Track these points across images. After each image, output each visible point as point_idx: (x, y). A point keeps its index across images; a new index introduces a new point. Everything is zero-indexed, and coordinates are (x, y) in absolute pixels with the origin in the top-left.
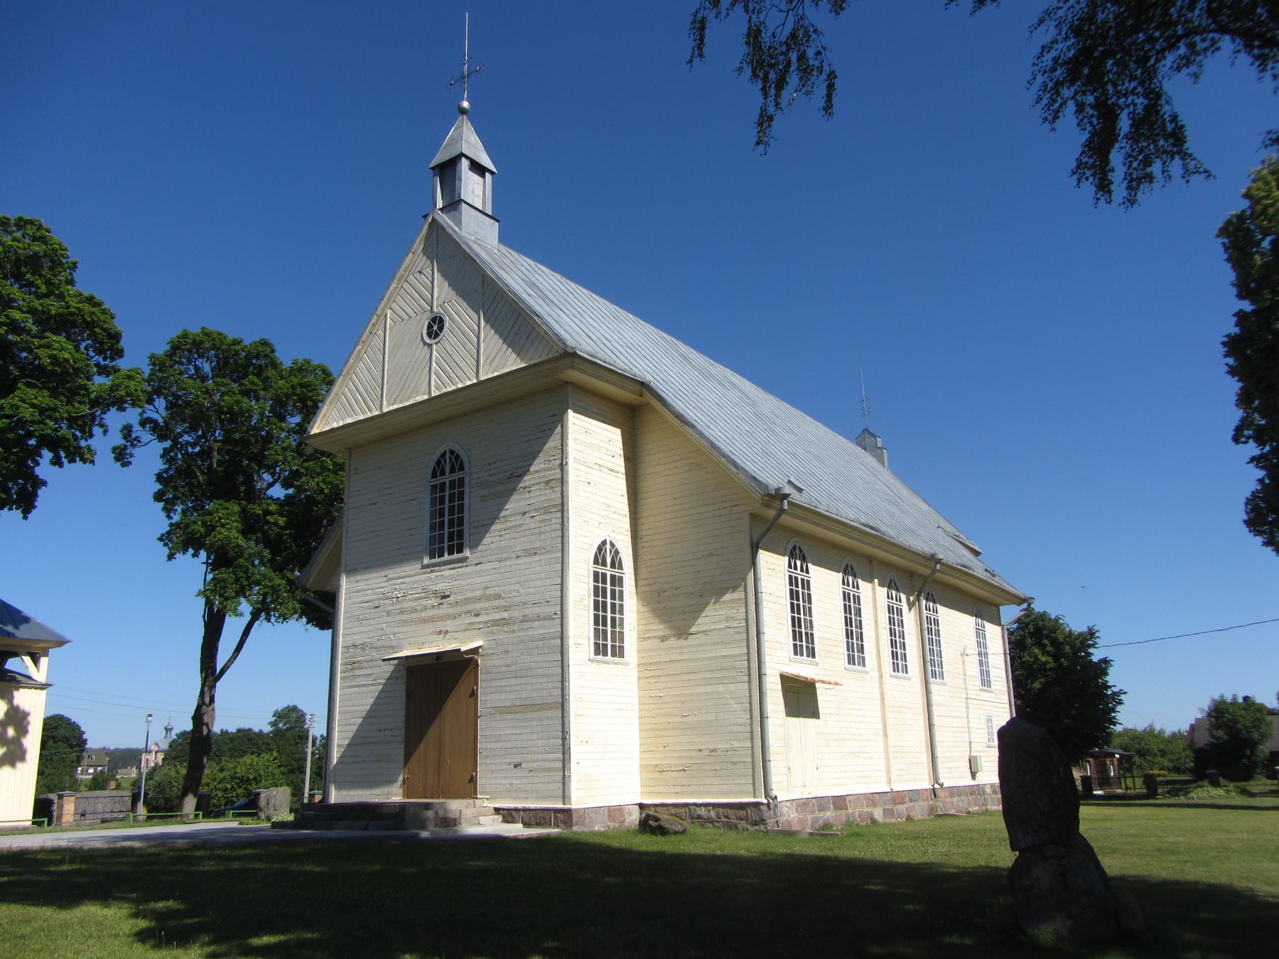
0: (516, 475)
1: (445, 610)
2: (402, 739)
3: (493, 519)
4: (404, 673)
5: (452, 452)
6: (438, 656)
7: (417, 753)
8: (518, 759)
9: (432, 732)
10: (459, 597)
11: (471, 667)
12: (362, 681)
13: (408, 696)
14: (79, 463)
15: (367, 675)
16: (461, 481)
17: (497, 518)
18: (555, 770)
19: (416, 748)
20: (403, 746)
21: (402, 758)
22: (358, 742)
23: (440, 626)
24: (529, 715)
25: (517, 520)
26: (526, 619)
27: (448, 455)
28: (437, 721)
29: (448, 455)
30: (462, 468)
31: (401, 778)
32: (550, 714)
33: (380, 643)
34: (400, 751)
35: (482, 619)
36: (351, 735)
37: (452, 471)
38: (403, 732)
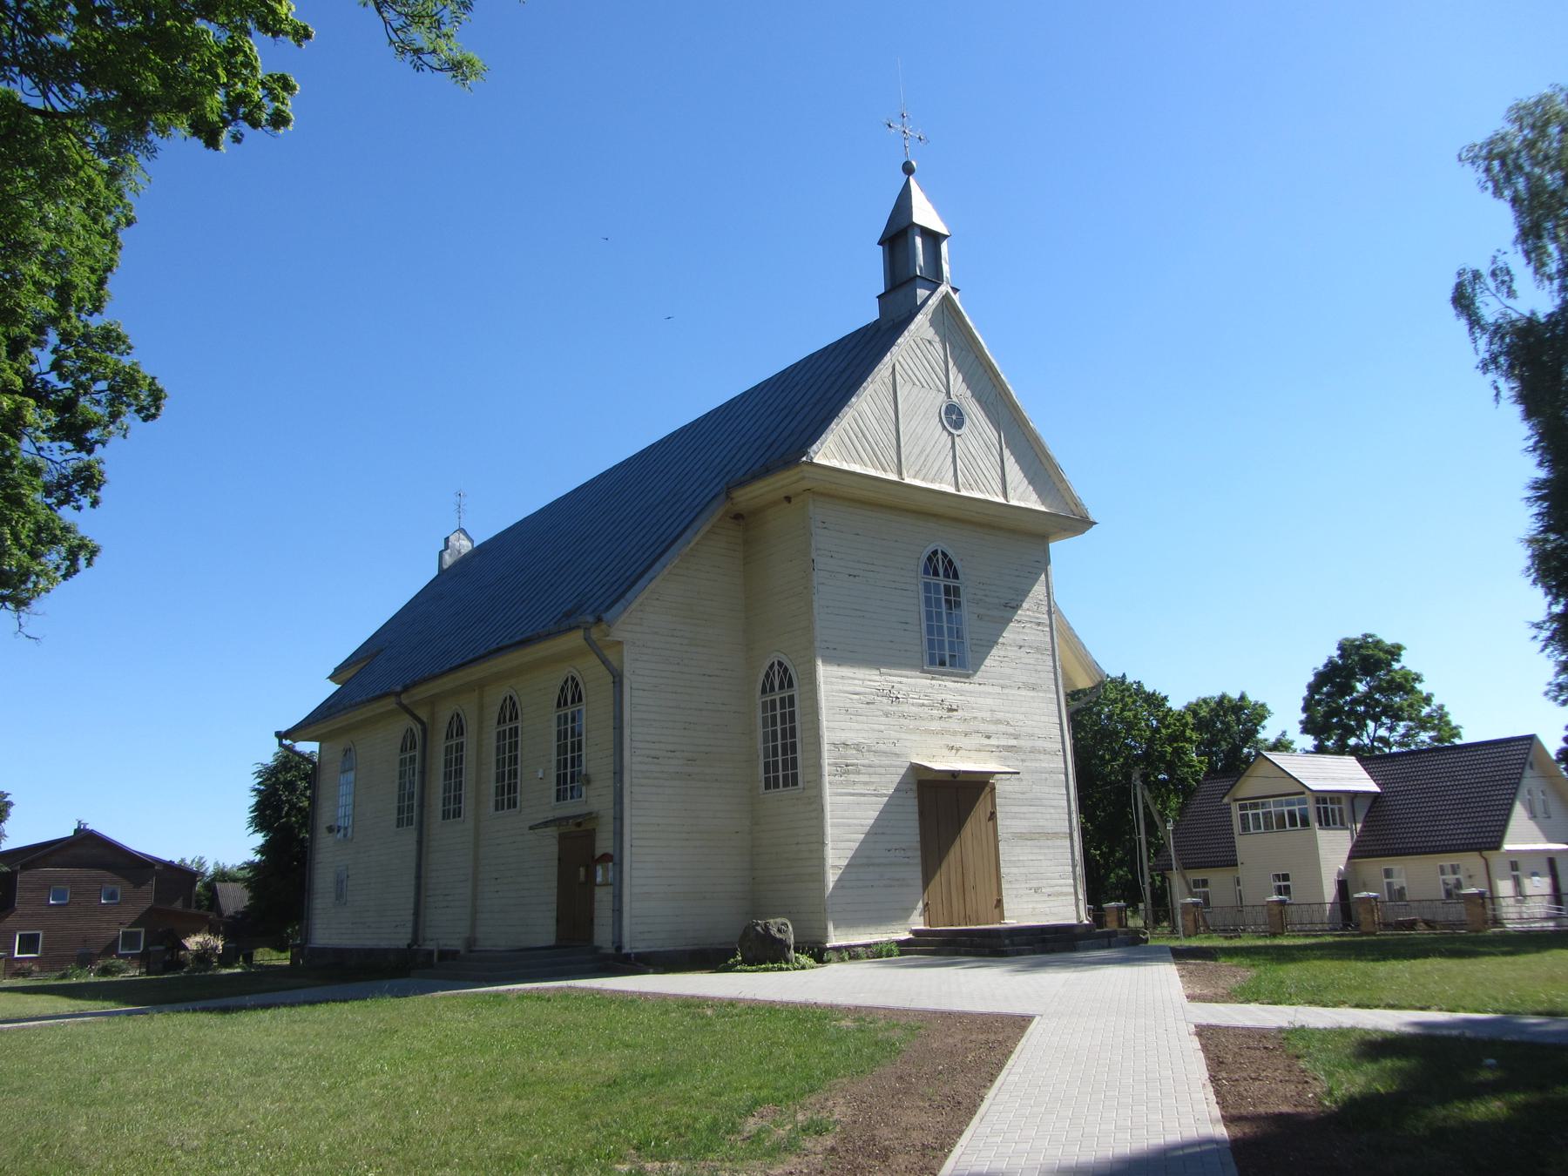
0: (1011, 606)
1: (953, 724)
2: (918, 860)
3: (992, 643)
4: (915, 787)
5: (780, 664)
6: (954, 774)
7: (937, 877)
8: (1034, 884)
9: (953, 854)
10: (967, 715)
11: (987, 789)
12: (859, 789)
13: (921, 814)
14: (200, 143)
15: (866, 783)
16: (791, 698)
17: (996, 642)
18: (1066, 894)
19: (934, 873)
20: (919, 868)
21: (920, 882)
22: (859, 863)
23: (951, 741)
24: (1049, 843)
25: (1012, 652)
26: (1033, 750)
27: (776, 667)
28: (957, 843)
29: (776, 667)
30: (791, 685)
31: (920, 905)
32: (1058, 842)
33: (882, 747)
34: (916, 874)
35: (993, 741)
36: (850, 854)
37: (781, 687)
38: (919, 853)
